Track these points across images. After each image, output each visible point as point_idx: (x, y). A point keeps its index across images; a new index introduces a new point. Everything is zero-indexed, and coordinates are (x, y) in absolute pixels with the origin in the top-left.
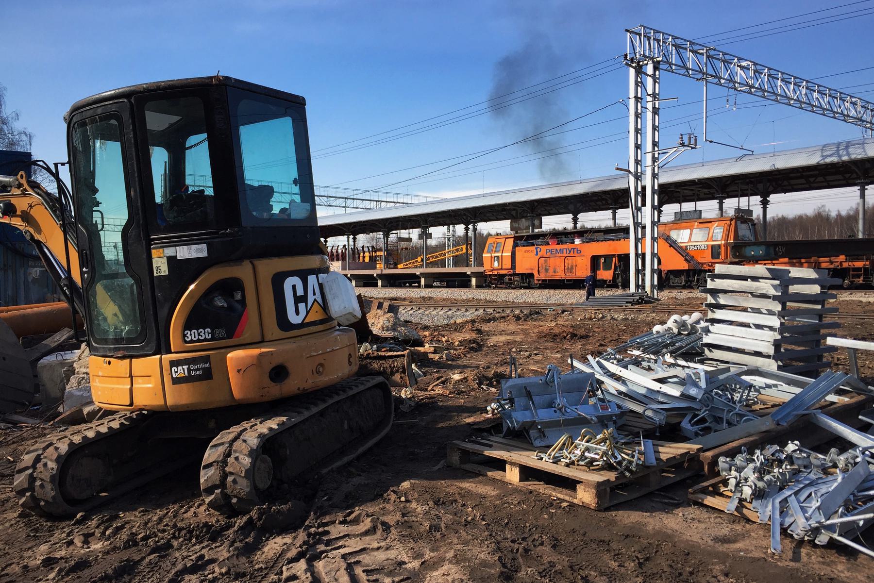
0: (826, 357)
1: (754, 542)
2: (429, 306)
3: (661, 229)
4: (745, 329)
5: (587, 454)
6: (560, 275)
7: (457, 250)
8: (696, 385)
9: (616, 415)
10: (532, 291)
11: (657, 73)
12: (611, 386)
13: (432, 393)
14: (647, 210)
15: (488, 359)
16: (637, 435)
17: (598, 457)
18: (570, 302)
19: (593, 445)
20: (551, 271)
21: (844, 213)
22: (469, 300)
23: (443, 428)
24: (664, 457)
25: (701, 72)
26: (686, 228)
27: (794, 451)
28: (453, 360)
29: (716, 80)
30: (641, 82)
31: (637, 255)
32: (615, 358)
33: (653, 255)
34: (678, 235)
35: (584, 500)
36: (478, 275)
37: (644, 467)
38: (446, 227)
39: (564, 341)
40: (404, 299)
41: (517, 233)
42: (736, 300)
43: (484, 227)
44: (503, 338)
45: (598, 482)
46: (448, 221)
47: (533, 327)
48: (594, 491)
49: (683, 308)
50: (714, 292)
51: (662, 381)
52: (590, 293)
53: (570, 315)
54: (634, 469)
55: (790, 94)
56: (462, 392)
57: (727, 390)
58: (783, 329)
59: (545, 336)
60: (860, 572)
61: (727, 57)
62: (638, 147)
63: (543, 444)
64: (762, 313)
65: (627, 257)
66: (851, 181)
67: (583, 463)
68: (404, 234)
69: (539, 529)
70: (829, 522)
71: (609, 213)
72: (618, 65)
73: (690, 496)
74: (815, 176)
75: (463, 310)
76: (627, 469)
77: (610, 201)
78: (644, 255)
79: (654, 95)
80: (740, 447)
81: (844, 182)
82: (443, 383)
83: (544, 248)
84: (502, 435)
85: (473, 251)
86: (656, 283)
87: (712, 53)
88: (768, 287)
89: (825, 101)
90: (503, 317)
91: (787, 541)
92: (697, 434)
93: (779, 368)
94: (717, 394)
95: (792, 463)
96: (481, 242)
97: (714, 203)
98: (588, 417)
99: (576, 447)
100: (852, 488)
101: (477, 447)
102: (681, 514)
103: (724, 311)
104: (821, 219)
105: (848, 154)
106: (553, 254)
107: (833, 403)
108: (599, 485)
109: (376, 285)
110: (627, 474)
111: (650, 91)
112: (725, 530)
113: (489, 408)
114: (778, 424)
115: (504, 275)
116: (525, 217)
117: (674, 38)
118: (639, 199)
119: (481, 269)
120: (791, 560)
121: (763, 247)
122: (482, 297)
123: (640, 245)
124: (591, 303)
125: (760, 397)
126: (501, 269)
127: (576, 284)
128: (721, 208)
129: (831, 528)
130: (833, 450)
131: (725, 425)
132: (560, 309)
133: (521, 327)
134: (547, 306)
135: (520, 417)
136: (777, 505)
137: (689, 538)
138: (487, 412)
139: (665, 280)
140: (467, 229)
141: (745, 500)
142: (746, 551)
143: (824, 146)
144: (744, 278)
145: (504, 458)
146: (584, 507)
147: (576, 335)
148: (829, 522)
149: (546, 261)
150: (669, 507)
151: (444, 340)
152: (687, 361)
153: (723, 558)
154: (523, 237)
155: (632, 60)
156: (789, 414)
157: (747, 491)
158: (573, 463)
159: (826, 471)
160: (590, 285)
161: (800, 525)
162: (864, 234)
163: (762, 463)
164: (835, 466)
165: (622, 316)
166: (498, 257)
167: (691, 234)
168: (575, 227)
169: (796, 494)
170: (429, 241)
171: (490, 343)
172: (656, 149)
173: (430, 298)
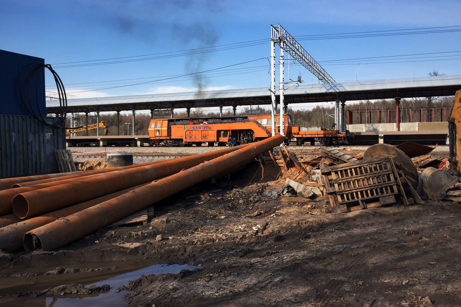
20: (193, 137)
71: (218, 108)
109: (136, 146)
126: (161, 137)
166: (159, 130)
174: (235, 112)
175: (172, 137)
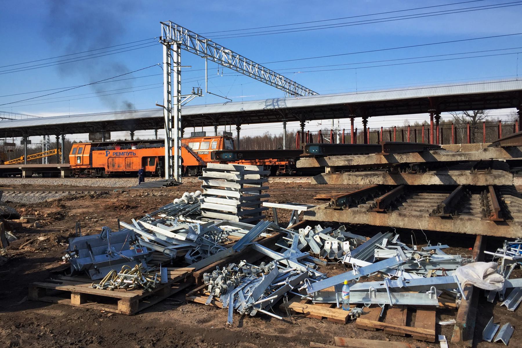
0: (264, 213)
1: (219, 320)
2: (28, 191)
3: (183, 141)
4: (222, 200)
5: (125, 281)
6: (122, 169)
7: (51, 152)
8: (194, 233)
9: (146, 255)
10: (104, 179)
11: (179, 50)
12: (146, 237)
13: (22, 251)
14: (175, 130)
15: (68, 225)
16: (158, 266)
17: (131, 282)
18: (129, 185)
19: (129, 275)
20: (116, 166)
21: (277, 136)
22: (59, 186)
23: (28, 274)
24: (172, 277)
25: (204, 53)
26: (197, 142)
27: (244, 266)
28: (42, 227)
29: (212, 59)
30: (170, 55)
31: (169, 157)
32: (150, 220)
33: (179, 157)
34: (193, 146)
35: (122, 310)
36: (66, 169)
37: (161, 284)
38: (42, 136)
39: (122, 211)
40: (9, 186)
41: (93, 141)
42: (218, 183)
43: (71, 137)
44: (80, 211)
45: (131, 298)
46: (48, 133)
47: (102, 203)
48: (129, 303)
49: (195, 188)
50: (207, 179)
51: (176, 232)
52: (142, 180)
53: (128, 193)
54: (154, 287)
55: (250, 71)
56: (45, 248)
57: (212, 234)
58: (242, 199)
59: (109, 208)
60: (271, 327)
61: (218, 46)
62: (169, 93)
63: (99, 278)
64: (232, 190)
65: (164, 157)
66: (279, 119)
67: (122, 287)
68: (9, 140)
69: (91, 333)
70: (257, 303)
71: (153, 132)
72: (156, 43)
73: (187, 298)
74: (263, 116)
75: (54, 192)
76: (150, 287)
77: (153, 124)
78: (173, 157)
79: (178, 63)
80: (215, 266)
81: (276, 120)
82: (31, 243)
83: (111, 152)
84: (70, 275)
85: (62, 153)
86: (180, 174)
87: (209, 43)
88: (234, 176)
89: (267, 76)
90: (82, 197)
91: (237, 317)
92: (193, 261)
93: (240, 220)
94: (206, 237)
95: (242, 272)
96: (68, 147)
97: (212, 128)
98: (129, 258)
99: (118, 277)
100: (269, 283)
101: (51, 285)
102: (181, 310)
103: (212, 189)
104: (267, 139)
105: (278, 105)
106: (117, 156)
107: (265, 237)
108: (132, 299)
110: (150, 290)
111: (175, 61)
112: (205, 316)
113: (63, 258)
114: (236, 252)
115: (85, 169)
116: (99, 132)
117: (189, 31)
118: (170, 123)
119: (68, 165)
120: (238, 327)
121: (231, 154)
122: (69, 184)
123: (171, 151)
124: (142, 186)
125: (229, 237)
126: (82, 165)
127: (132, 174)
128: (216, 131)
129: (257, 306)
130: (262, 263)
131: (209, 254)
132: (121, 190)
133: (93, 202)
134: (113, 189)
135: (82, 262)
136: (233, 297)
137: (184, 323)
138: (62, 260)
139: (186, 171)
140: (58, 138)
141: (217, 296)
142: (215, 325)
143: (267, 100)
144: (223, 171)
145: (70, 290)
146: (123, 314)
147: (129, 207)
148: (257, 303)
149: (113, 160)
150: (174, 306)
151: (36, 213)
152: (192, 219)
153: (201, 331)
154: (97, 144)
155: (164, 41)
156: (242, 245)
157: (218, 291)
158: (116, 288)
159: (259, 275)
160: (141, 175)
161: (243, 305)
162: (285, 147)
163: (226, 274)
164: (263, 271)
165: (159, 194)
166: (80, 157)
167: (200, 145)
168: (132, 139)
169: (243, 289)
170: (29, 146)
171: (71, 214)
172: (180, 95)
173: (30, 185)
174: (365, 126)
175: (93, 167)
